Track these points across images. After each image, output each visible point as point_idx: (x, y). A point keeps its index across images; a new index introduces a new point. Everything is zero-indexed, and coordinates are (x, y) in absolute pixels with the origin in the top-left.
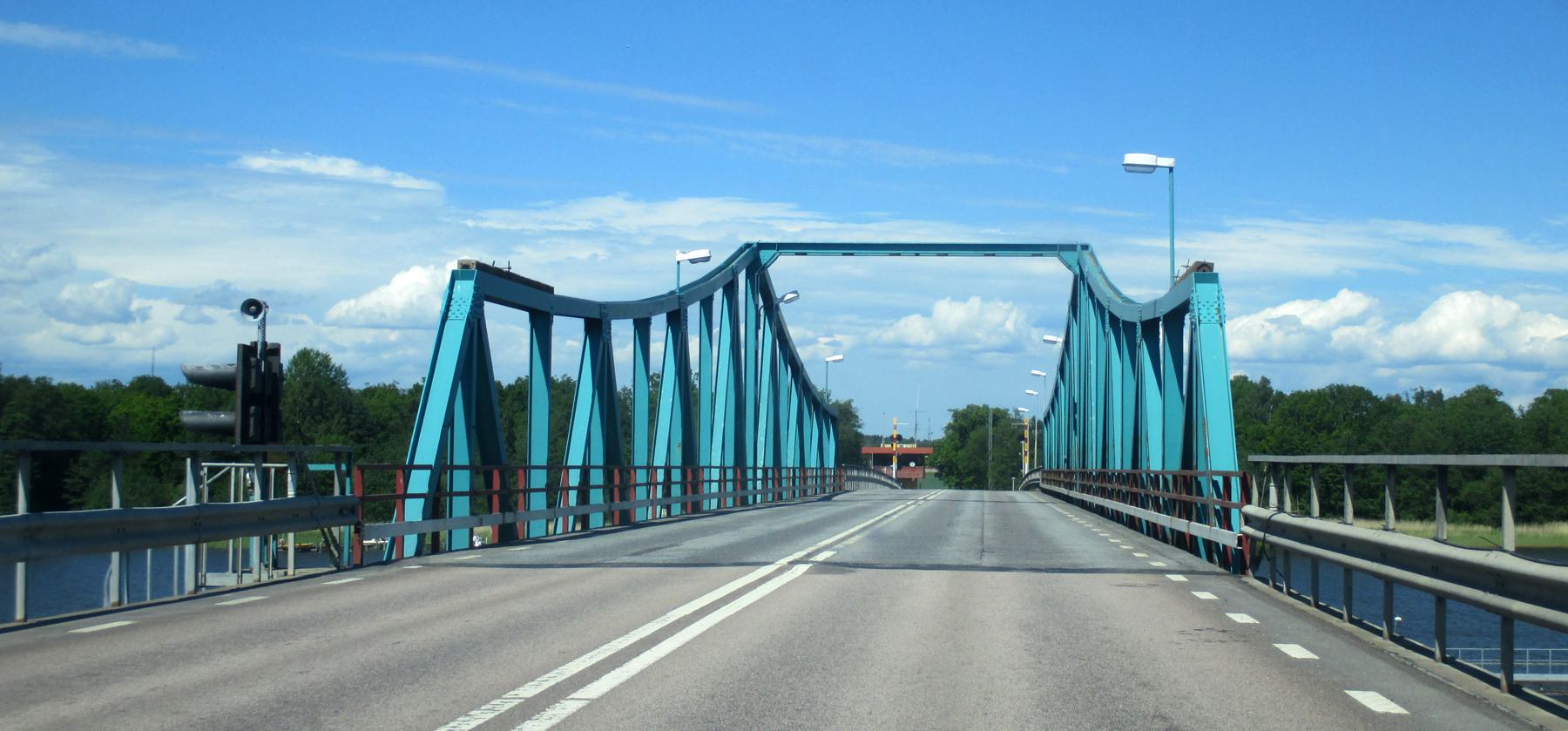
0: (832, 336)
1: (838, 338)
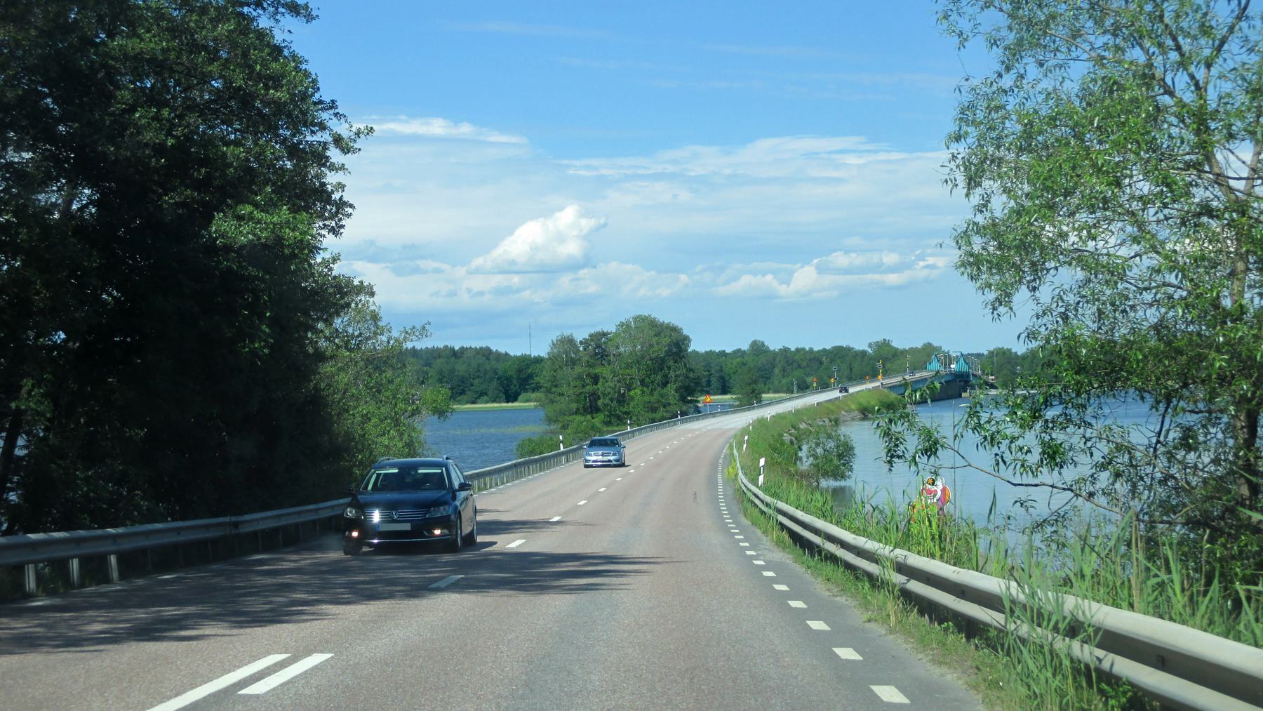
0: (924, 260)
1: (931, 261)
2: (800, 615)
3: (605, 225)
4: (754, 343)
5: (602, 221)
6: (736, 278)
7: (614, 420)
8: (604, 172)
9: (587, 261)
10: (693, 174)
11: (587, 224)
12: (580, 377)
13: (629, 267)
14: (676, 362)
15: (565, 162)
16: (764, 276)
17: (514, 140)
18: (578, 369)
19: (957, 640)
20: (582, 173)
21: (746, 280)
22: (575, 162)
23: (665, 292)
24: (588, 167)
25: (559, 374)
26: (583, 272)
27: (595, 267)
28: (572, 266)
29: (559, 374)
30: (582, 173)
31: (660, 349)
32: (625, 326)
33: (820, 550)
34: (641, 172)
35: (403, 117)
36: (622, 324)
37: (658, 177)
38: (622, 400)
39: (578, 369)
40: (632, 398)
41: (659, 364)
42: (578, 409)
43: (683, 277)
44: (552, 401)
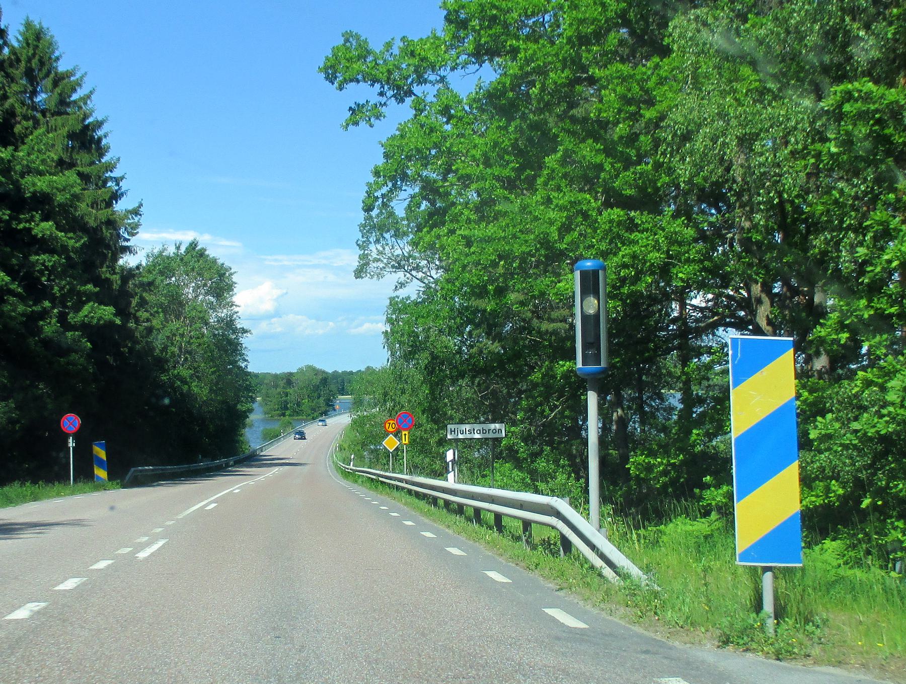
2: (387, 512)
3: (287, 293)
4: (368, 368)
5: (285, 291)
6: (361, 325)
7: (295, 414)
8: (286, 263)
9: (277, 314)
10: (335, 265)
11: (277, 292)
12: (279, 393)
13: (300, 317)
14: (324, 387)
15: (263, 257)
16: (377, 323)
17: (234, 244)
18: (279, 390)
19: (422, 504)
20: (273, 263)
21: (367, 326)
22: (269, 257)
23: (321, 332)
24: (276, 260)
25: (270, 391)
26: (274, 320)
27: (280, 317)
28: (268, 317)
29: (270, 391)
30: (273, 263)
31: (316, 381)
32: (301, 371)
33: (407, 483)
34: (307, 263)
35: (171, 230)
36: (299, 369)
37: (315, 267)
38: (298, 404)
39: (279, 390)
40: (304, 404)
41: (316, 388)
42: (85, 103)
43: (331, 323)
44: (266, 404)
